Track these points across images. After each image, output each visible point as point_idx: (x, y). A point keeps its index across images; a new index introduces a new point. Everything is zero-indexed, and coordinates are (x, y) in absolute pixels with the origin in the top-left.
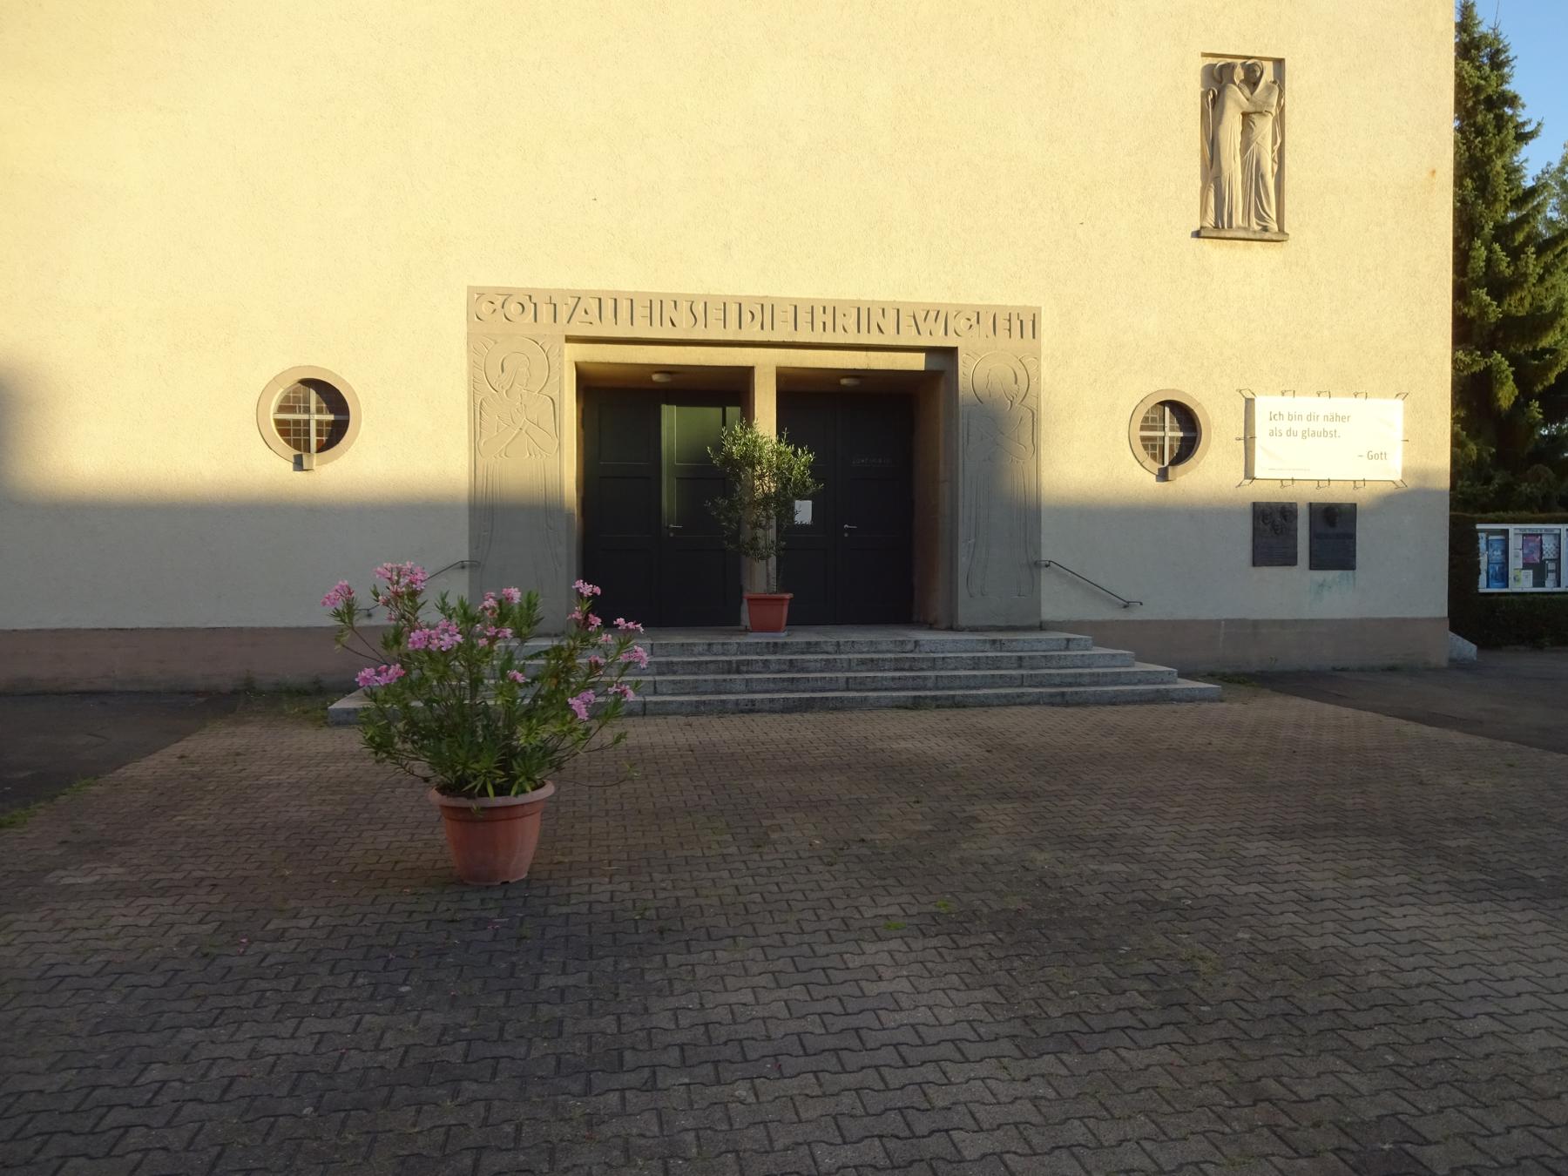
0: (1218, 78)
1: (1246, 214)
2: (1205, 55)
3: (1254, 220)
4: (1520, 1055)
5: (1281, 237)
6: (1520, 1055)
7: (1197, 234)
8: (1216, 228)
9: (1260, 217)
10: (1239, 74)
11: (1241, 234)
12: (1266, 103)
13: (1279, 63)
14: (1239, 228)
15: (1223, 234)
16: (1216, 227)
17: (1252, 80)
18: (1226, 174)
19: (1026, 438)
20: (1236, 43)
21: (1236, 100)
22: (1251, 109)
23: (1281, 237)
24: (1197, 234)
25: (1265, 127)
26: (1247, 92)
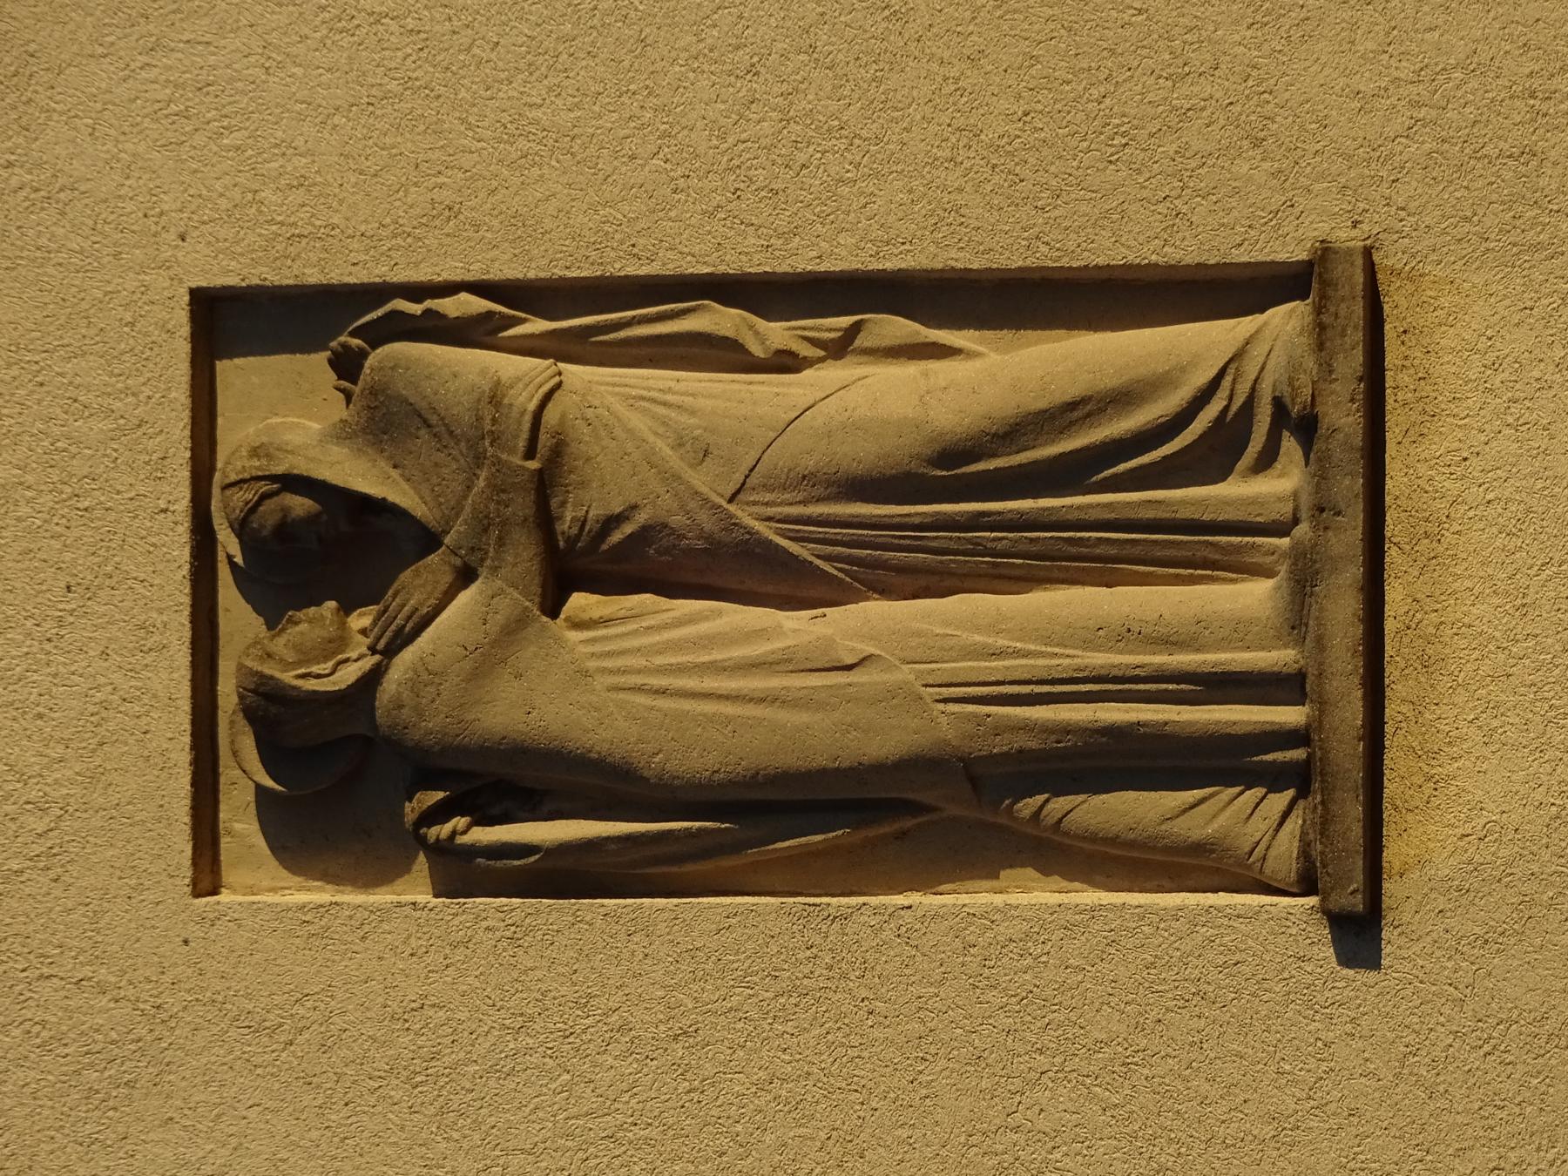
0: (341, 785)
1: (1206, 549)
2: (207, 873)
3: (1239, 491)
4: (693, 395)
5: (1346, 295)
6: (693, 395)
7: (1358, 934)
8: (1305, 789)
9: (1219, 453)
10: (323, 650)
11: (1341, 607)
12: (473, 435)
13: (227, 322)
14: (1299, 618)
15: (1346, 752)
16: (1300, 779)
17: (312, 548)
18: (947, 725)
19: (1249, 729)
20: (109, 659)
21: (461, 656)
22: (523, 556)
23: (1346, 295)
24: (1358, 934)
25: (641, 424)
26: (417, 583)
